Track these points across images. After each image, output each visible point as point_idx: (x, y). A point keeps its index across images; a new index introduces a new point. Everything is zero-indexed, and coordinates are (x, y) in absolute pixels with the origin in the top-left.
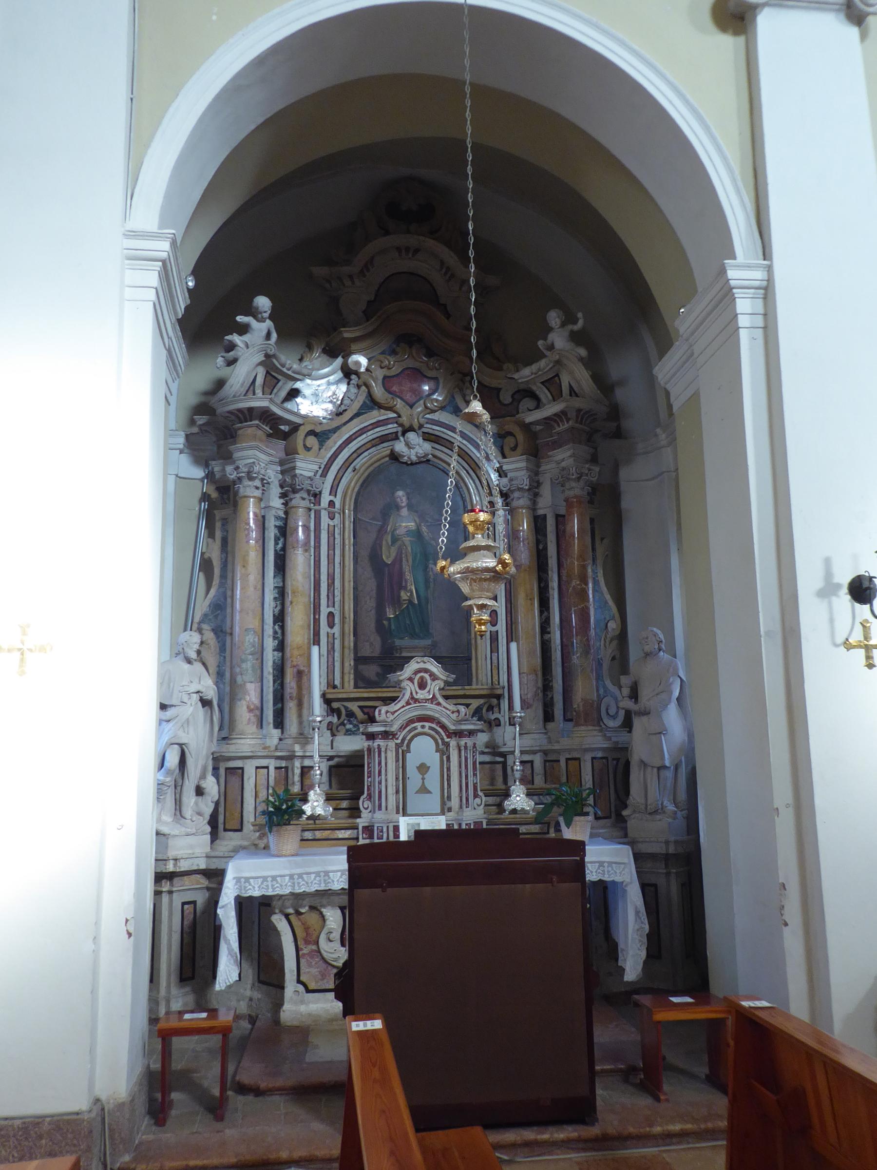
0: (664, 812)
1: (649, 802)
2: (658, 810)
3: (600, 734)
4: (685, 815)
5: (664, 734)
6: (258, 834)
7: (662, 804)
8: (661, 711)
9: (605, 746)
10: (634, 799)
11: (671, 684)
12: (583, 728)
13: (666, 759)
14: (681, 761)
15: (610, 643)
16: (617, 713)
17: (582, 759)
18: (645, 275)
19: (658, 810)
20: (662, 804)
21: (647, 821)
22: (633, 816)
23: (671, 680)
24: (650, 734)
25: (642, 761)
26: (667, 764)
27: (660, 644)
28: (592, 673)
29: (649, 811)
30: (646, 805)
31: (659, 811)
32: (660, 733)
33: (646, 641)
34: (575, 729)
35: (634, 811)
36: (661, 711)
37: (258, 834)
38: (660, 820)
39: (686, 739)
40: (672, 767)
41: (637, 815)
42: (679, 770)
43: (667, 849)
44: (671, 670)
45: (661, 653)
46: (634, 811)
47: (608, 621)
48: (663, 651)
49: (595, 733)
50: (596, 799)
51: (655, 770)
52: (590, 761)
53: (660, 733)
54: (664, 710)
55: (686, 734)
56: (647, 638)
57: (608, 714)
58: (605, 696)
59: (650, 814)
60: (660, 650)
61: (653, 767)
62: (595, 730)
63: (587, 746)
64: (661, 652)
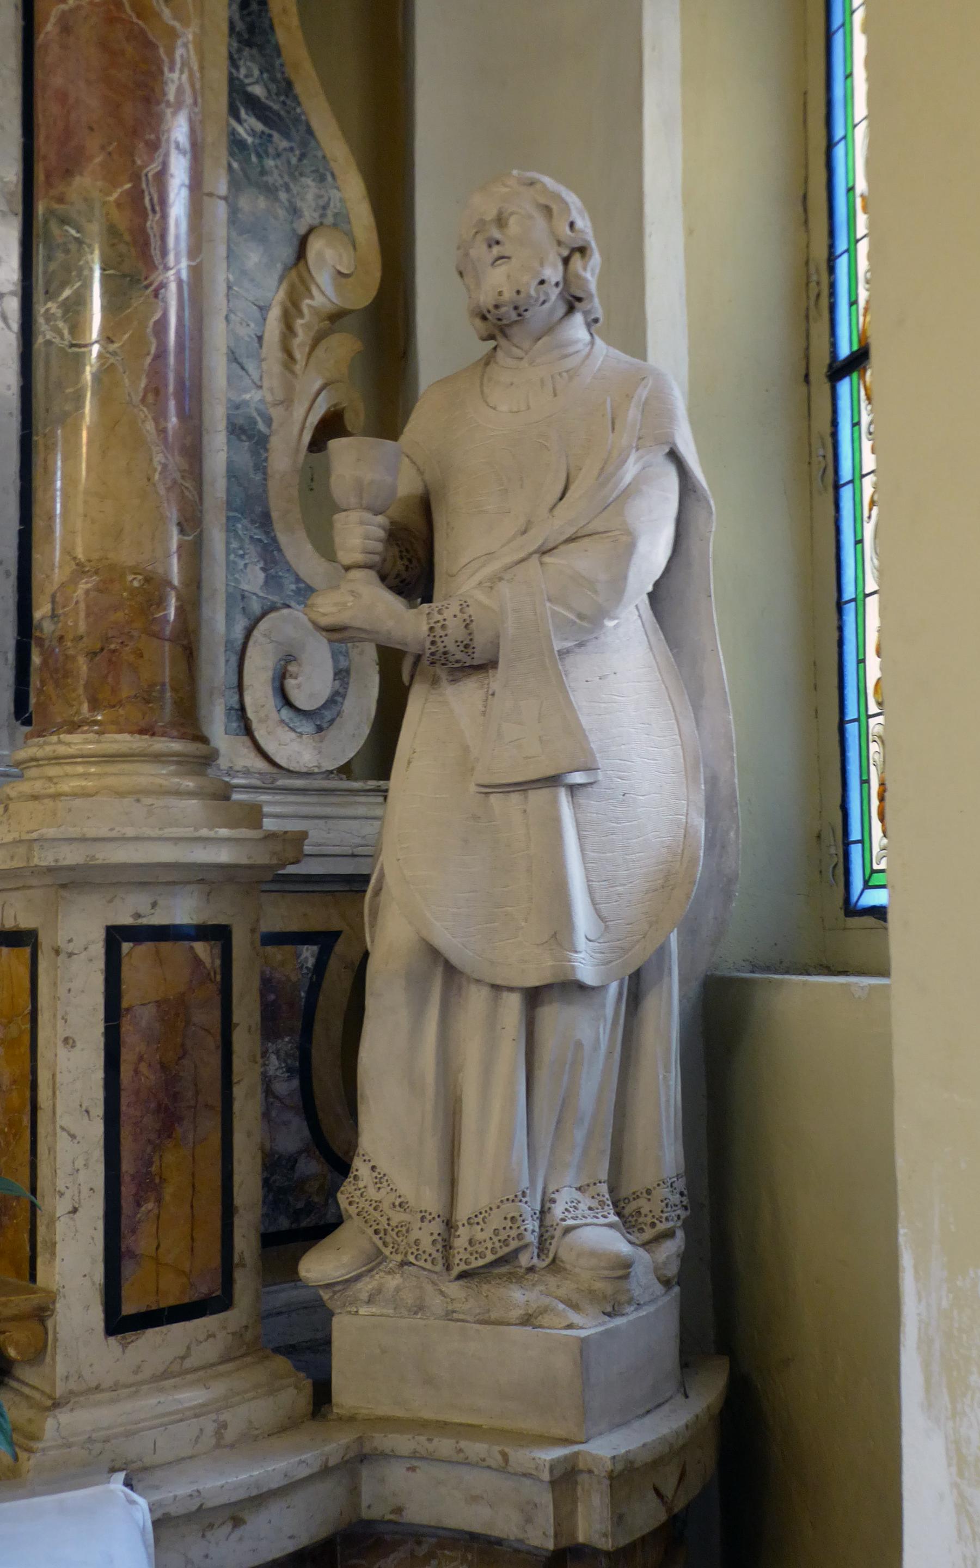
0: (555, 1266)
1: (463, 1211)
2: (516, 1252)
3: (189, 784)
4: (672, 1270)
5: (573, 789)
6: (287, 1075)
7: (544, 1212)
8: (564, 653)
9: (224, 856)
10: (380, 1180)
11: (629, 493)
12: (77, 742)
13: (581, 943)
14: (662, 951)
15: (316, 342)
16: (334, 700)
17: (44, 940)
18: (683, 1153)
19: (516, 1252)
20: (544, 1212)
21: (449, 1316)
22: (365, 1287)
23: (631, 470)
24: (489, 789)
25: (434, 954)
26: (587, 971)
27: (576, 261)
28: (160, 415)
29: (462, 1258)
30: (450, 1225)
31: (524, 1260)
32: (553, 781)
33: (497, 234)
34: (22, 754)
35: (375, 1260)
36: (564, 653)
37: (287, 1075)
38: (527, 1320)
39: (700, 823)
40: (613, 988)
41: (393, 1282)
42: (651, 1005)
43: (563, 1520)
44: (633, 413)
45: (577, 328)
46: (375, 1260)
47: (311, 230)
48: (592, 323)
49: (160, 775)
50: (128, 1190)
51: (513, 1004)
52: (98, 949)
53: (553, 781)
54: (581, 645)
55: (699, 799)
56: (501, 221)
57: (286, 700)
58: (273, 608)
59: (463, 1276)
60: (572, 303)
61: (496, 988)
62: (158, 758)
63: (71, 856)
64: (578, 319)
